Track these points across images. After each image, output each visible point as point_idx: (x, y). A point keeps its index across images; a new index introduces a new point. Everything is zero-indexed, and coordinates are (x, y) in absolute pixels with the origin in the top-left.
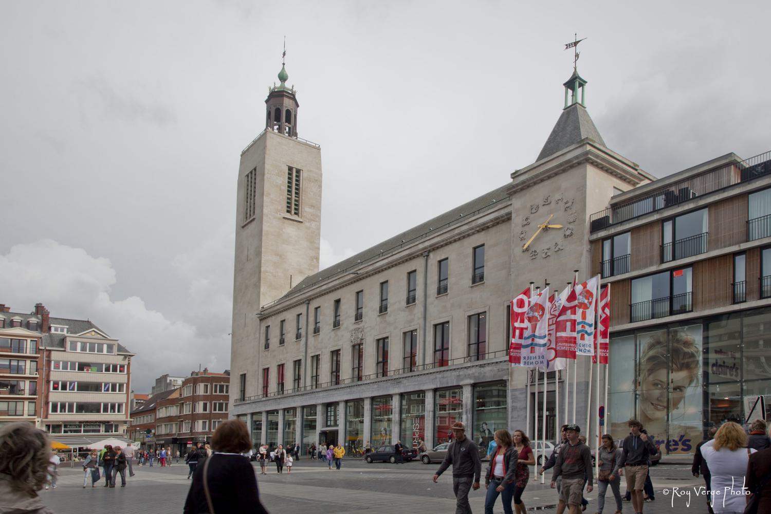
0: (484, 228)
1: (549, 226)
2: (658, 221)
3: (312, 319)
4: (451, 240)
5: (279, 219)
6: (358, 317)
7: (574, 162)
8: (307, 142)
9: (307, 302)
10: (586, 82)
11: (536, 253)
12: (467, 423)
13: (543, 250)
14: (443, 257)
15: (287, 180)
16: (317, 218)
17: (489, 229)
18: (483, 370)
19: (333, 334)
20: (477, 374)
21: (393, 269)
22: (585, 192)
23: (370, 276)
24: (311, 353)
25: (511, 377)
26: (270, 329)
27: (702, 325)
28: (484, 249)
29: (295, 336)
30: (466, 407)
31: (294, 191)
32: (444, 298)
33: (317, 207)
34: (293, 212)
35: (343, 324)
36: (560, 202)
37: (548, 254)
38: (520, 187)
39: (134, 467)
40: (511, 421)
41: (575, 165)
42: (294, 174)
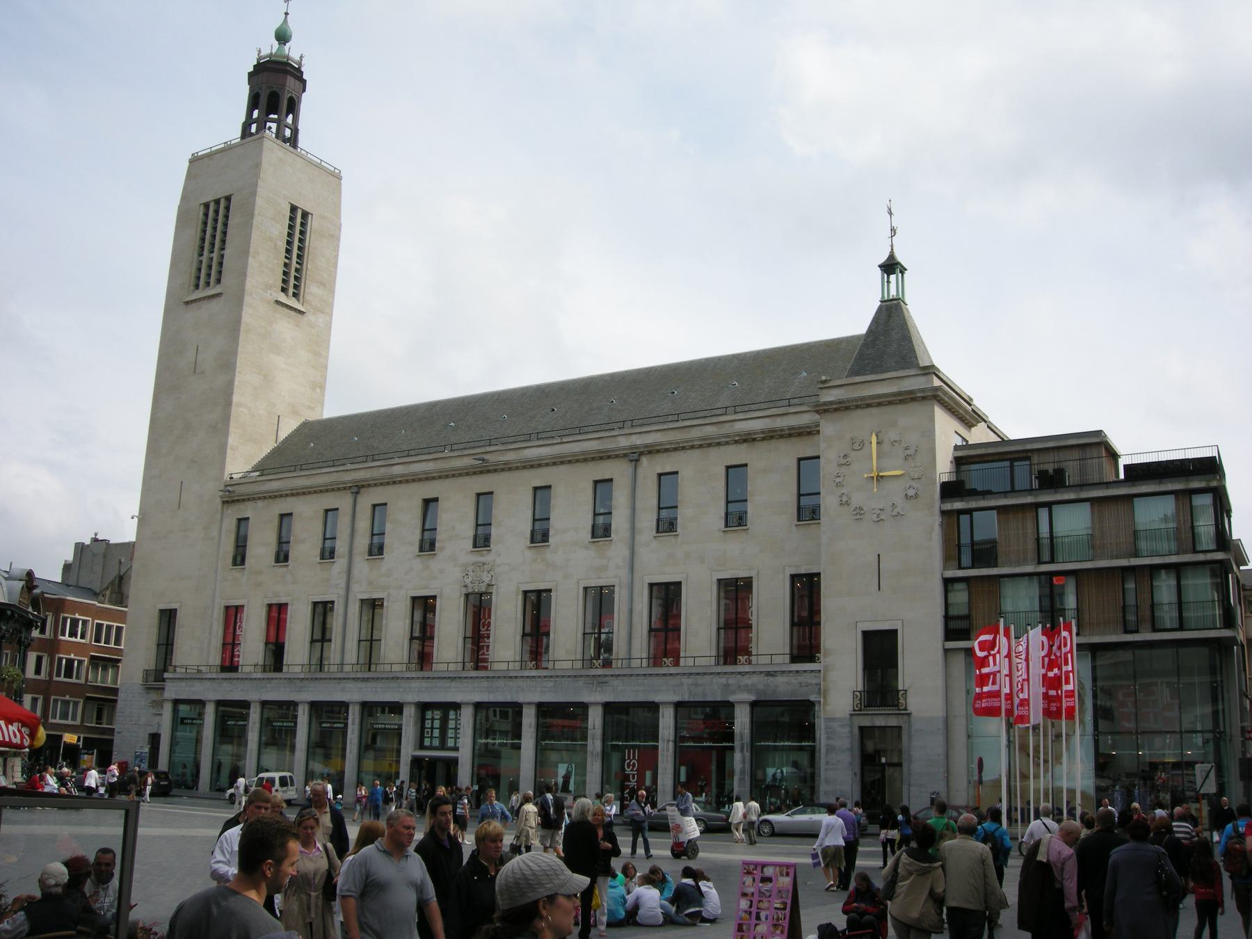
0: (747, 439)
1: (881, 474)
2: (1031, 504)
3: (363, 525)
4: (686, 445)
5: (269, 302)
6: (482, 541)
7: (919, 395)
8: (323, 163)
9: (355, 489)
10: (906, 270)
11: (862, 512)
12: (744, 767)
13: (874, 509)
14: (668, 470)
15: (286, 230)
16: (326, 308)
17: (756, 443)
18: (772, 681)
19: (417, 564)
20: (761, 687)
21: (562, 468)
22: (934, 440)
23: (510, 469)
24: (361, 591)
25: (825, 698)
27: (1090, 654)
29: (318, 551)
30: (742, 738)
31: (295, 251)
32: (668, 539)
33: (329, 285)
34: (291, 290)
35: (442, 549)
36: (896, 444)
37: (882, 517)
38: (834, 406)
39: (647, 834)
40: (826, 770)
41: (918, 399)
42: (299, 220)
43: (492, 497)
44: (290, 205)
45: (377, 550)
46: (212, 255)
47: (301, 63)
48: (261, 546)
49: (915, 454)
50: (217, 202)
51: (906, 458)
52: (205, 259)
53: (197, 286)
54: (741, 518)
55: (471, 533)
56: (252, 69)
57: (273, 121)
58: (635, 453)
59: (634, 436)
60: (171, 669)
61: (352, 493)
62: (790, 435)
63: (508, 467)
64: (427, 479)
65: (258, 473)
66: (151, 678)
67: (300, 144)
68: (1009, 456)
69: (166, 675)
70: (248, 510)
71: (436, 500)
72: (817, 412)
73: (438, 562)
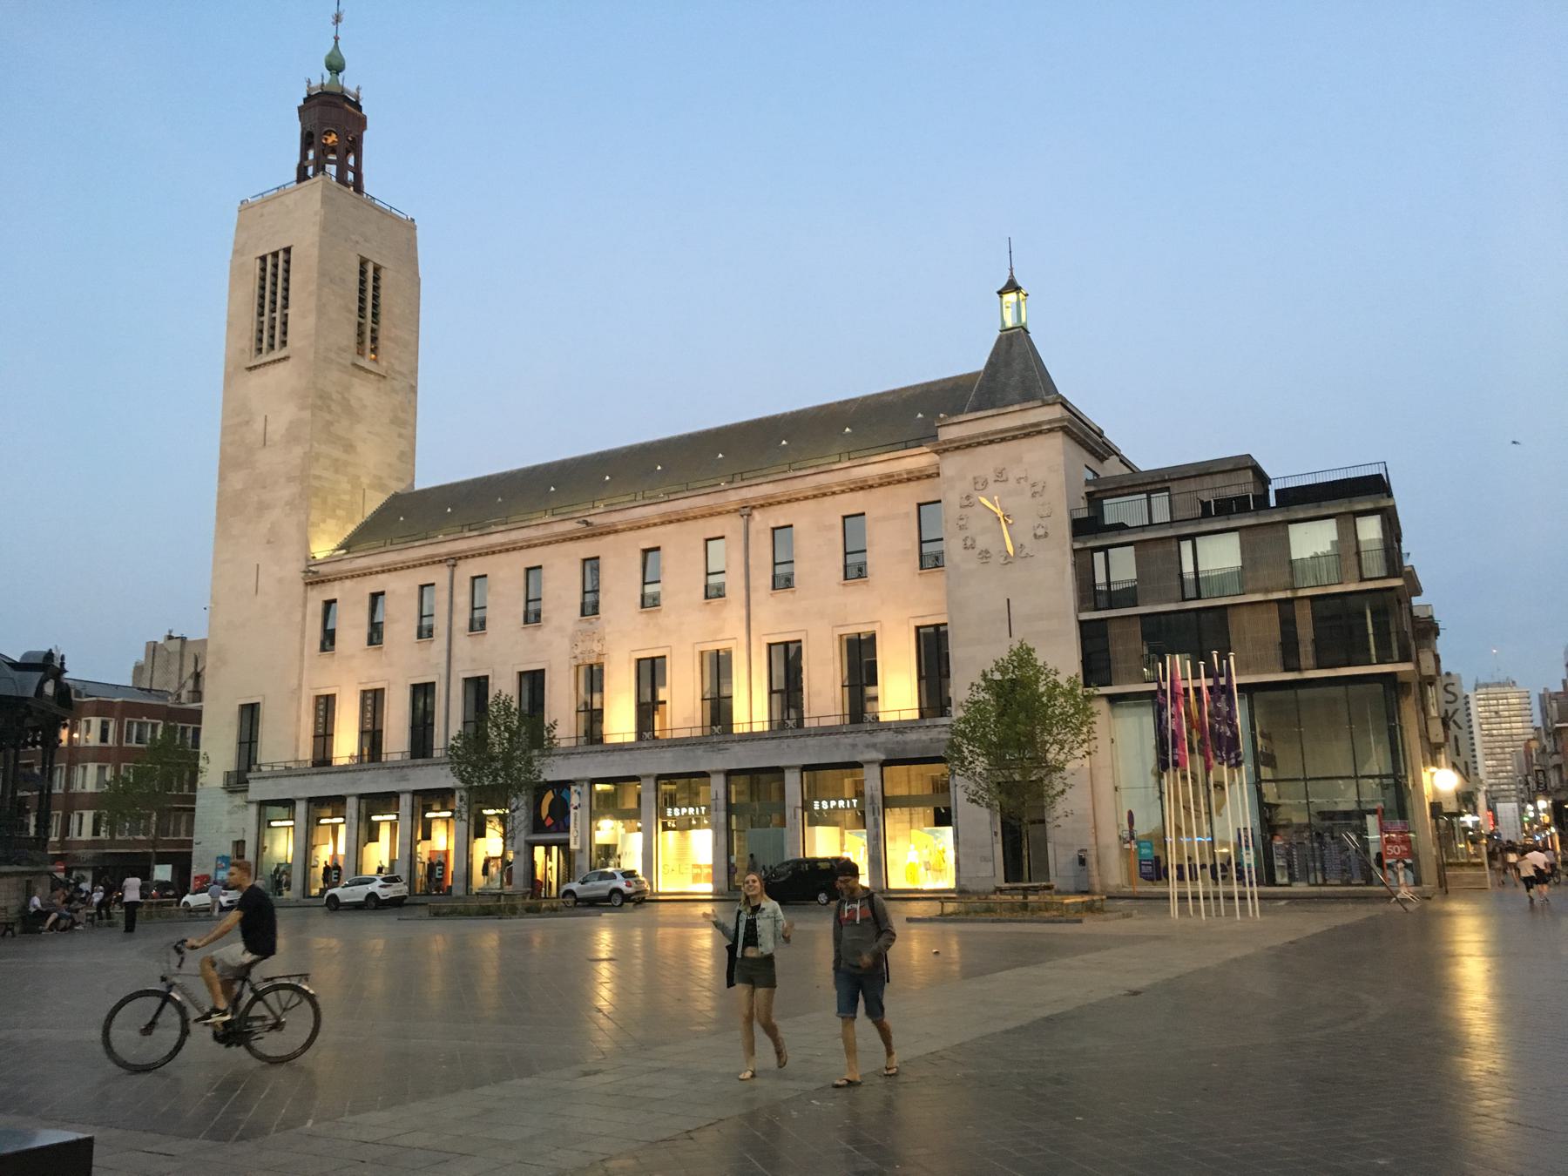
0: (863, 486)
3: (462, 600)
6: (590, 609)
7: (1045, 427)
9: (452, 562)
11: (988, 555)
17: (873, 490)
24: (463, 670)
26: (338, 609)
28: (864, 520)
32: (783, 594)
36: (1022, 480)
42: (370, 274)
43: (541, 574)
44: (359, 258)
45: (477, 625)
46: (274, 315)
47: (358, 97)
48: (351, 626)
49: (1043, 490)
50: (275, 255)
51: (1034, 495)
52: (266, 319)
53: (260, 350)
54: (860, 570)
55: (578, 601)
56: (302, 103)
57: (331, 162)
58: (746, 507)
59: (745, 489)
60: (254, 768)
61: (448, 566)
62: (909, 480)
63: (612, 531)
64: (529, 547)
65: (343, 551)
66: (232, 781)
67: (366, 189)
68: (1145, 488)
69: (249, 775)
70: (332, 591)
71: (383, 593)
72: (936, 452)
73: (544, 634)
